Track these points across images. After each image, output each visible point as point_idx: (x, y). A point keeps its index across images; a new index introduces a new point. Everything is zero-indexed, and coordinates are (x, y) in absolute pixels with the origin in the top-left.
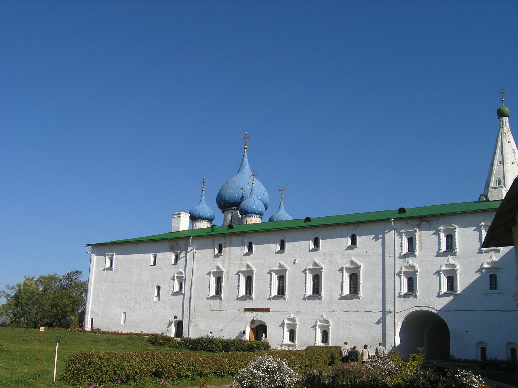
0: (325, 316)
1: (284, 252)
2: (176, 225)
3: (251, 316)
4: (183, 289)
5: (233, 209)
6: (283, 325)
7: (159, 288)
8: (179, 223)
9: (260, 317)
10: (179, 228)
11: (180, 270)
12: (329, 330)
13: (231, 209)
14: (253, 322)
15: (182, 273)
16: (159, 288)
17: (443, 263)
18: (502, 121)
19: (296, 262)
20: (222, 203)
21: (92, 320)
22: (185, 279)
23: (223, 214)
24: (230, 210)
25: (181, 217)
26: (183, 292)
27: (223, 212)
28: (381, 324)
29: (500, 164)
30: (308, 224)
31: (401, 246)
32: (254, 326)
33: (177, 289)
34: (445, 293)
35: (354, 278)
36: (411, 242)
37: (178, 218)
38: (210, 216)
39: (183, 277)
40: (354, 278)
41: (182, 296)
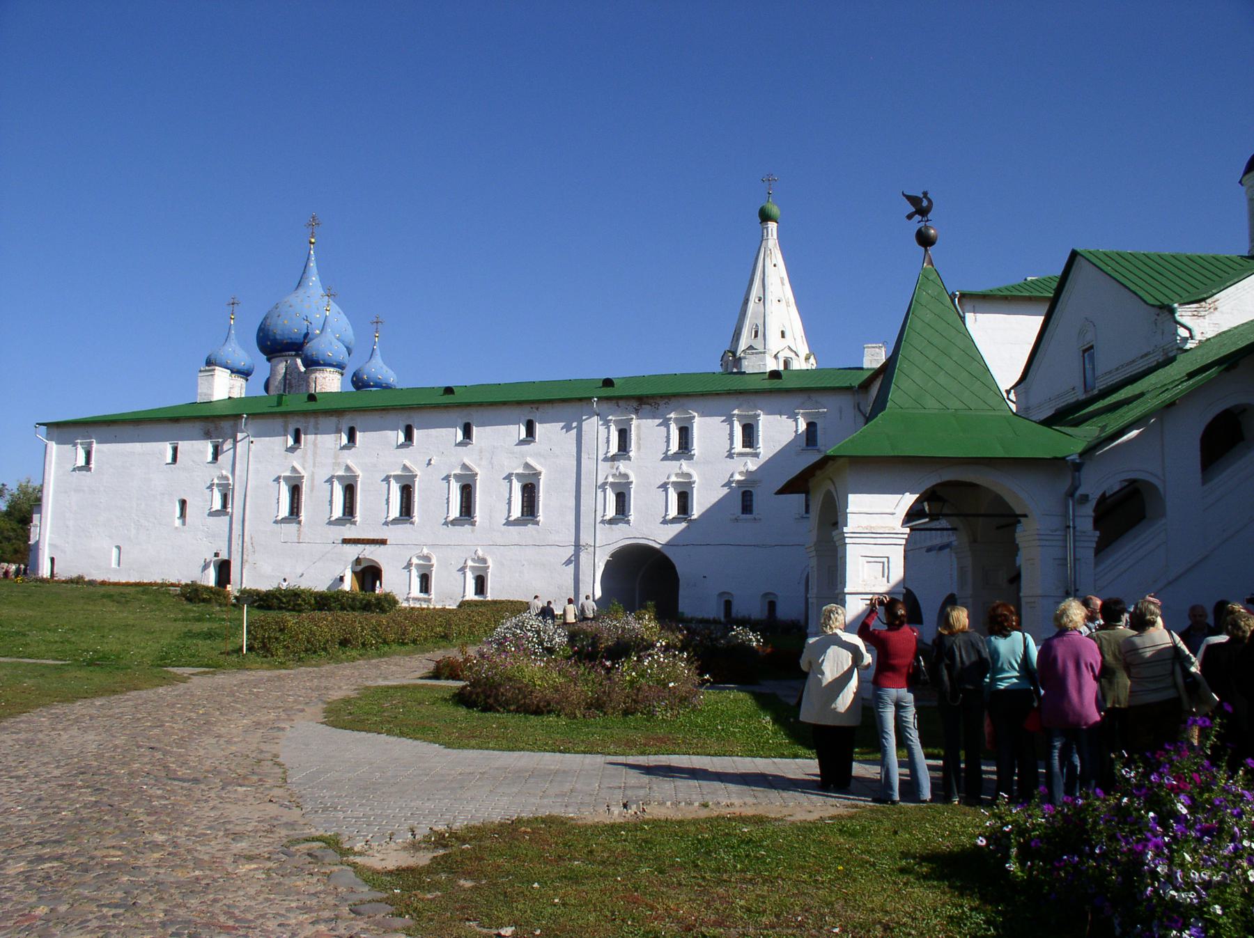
0: (480, 553)
1: (411, 445)
2: (205, 391)
3: (354, 551)
4: (230, 506)
6: (409, 566)
7: (183, 503)
8: (211, 387)
9: (370, 553)
10: (212, 395)
12: (487, 575)
14: (358, 561)
15: (227, 478)
16: (183, 503)
17: (213, 474)
18: (767, 228)
19: (432, 462)
20: (269, 343)
21: (52, 560)
22: (233, 489)
23: (268, 365)
24: (283, 356)
25: (216, 377)
26: (229, 510)
27: (269, 360)
28: (572, 566)
29: (759, 300)
30: (449, 399)
31: (608, 442)
32: (359, 568)
33: (217, 505)
34: (673, 518)
35: (530, 492)
36: (624, 435)
37: (210, 377)
38: (245, 368)
39: (229, 484)
40: (530, 492)
41: (227, 518)
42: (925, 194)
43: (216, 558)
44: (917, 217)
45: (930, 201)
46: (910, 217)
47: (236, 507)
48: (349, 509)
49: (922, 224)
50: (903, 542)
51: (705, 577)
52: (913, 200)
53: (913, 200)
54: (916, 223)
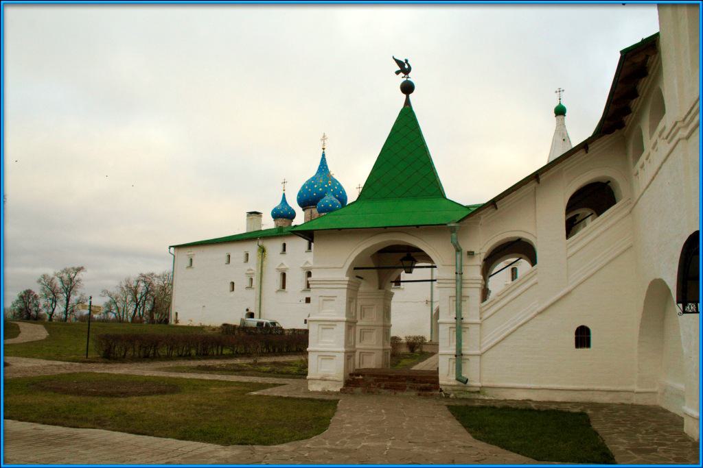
10: (261, 225)
27: (304, 210)
42: (406, 61)
44: (402, 74)
45: (409, 65)
46: (397, 73)
49: (405, 79)
50: (346, 286)
51: (583, 337)
52: (399, 63)
53: (399, 63)
54: (401, 79)
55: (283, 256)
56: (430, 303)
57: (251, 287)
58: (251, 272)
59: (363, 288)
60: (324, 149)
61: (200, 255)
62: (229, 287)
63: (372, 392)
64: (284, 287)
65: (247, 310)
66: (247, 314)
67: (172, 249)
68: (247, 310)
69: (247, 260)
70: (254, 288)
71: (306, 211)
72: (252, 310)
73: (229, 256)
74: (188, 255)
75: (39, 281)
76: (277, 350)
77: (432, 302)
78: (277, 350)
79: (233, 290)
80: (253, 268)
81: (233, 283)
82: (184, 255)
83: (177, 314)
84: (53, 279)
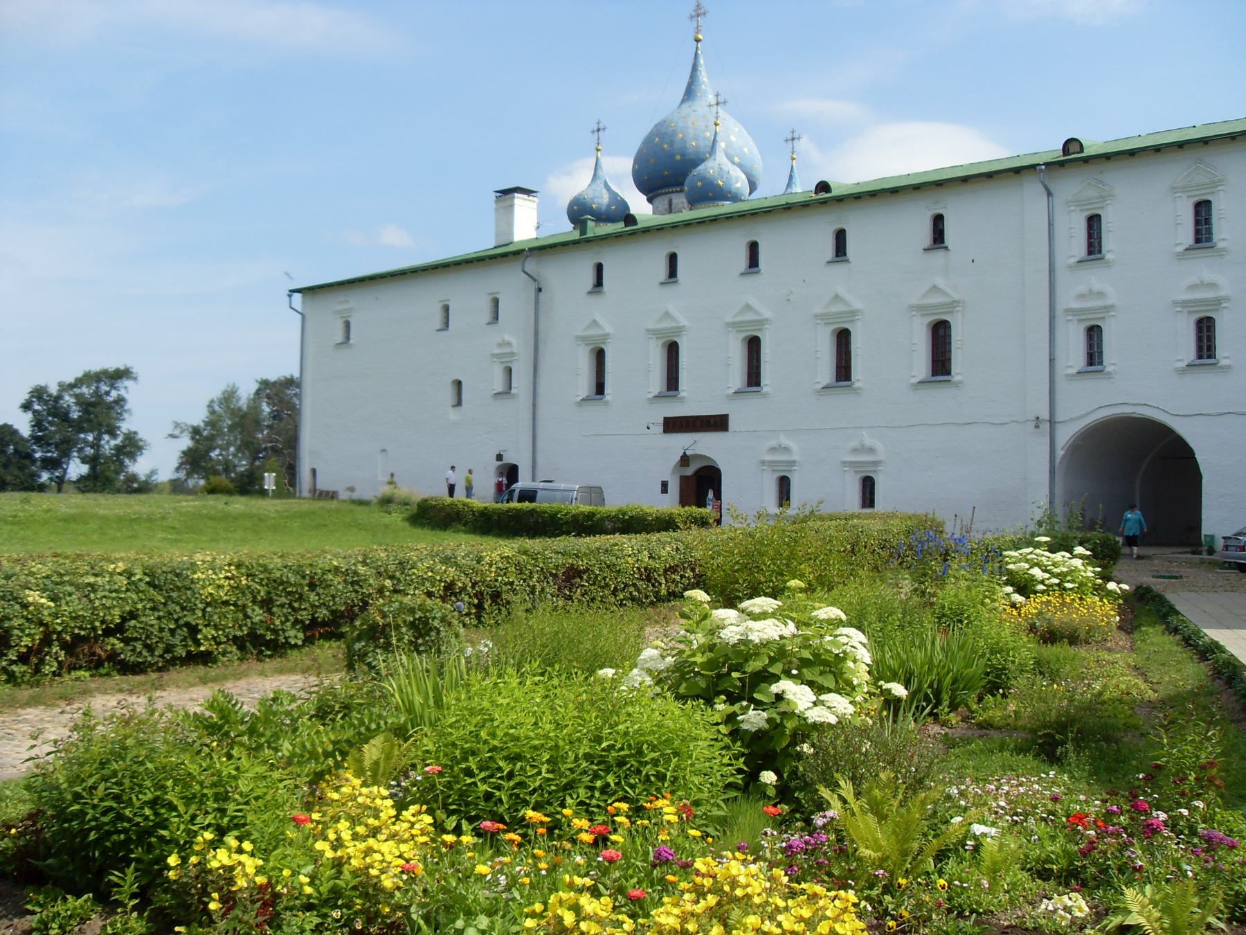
1: (758, 272)
5: (672, 192)
10: (511, 234)
11: (507, 338)
13: (669, 193)
14: (685, 460)
24: (666, 193)
25: (517, 209)
27: (650, 200)
32: (689, 471)
43: (500, 463)
47: (521, 382)
48: (672, 382)
55: (594, 300)
56: (1046, 427)
57: (508, 390)
58: (507, 350)
59: (709, 135)
60: (716, 124)
61: (363, 308)
62: (448, 394)
63: (840, 840)
64: (600, 388)
65: (499, 457)
66: (500, 467)
67: (297, 296)
68: (499, 457)
69: (496, 317)
70: (514, 396)
71: (657, 201)
72: (509, 459)
73: (446, 309)
74: (338, 312)
75: (26, 407)
76: (281, 837)
77: (1052, 422)
78: (281, 837)
79: (459, 403)
80: (513, 341)
81: (458, 384)
82: (330, 311)
83: (314, 472)
84: (59, 398)
